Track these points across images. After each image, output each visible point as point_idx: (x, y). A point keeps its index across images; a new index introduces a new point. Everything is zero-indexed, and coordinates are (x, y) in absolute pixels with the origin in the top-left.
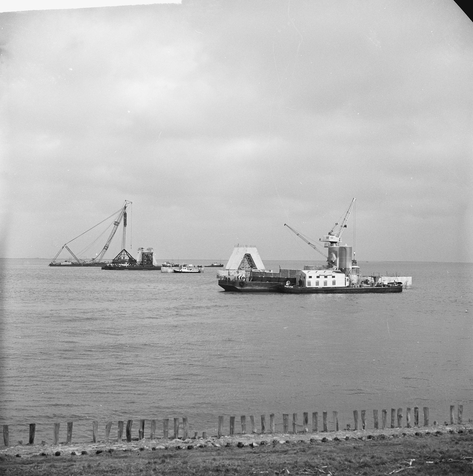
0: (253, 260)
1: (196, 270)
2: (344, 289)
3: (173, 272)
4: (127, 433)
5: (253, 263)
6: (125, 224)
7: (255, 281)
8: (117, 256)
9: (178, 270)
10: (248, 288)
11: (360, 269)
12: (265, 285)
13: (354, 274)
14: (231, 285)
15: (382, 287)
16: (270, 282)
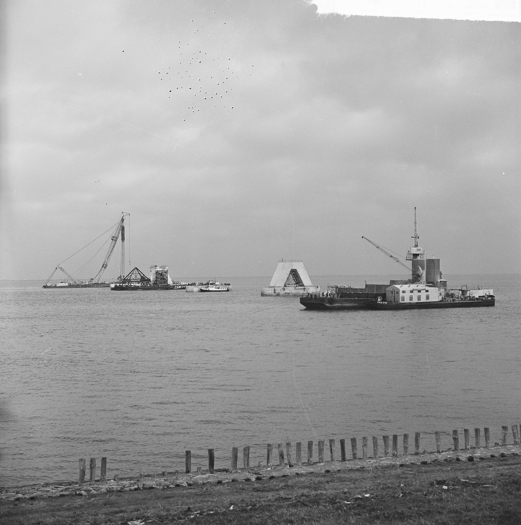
0: (299, 276)
1: (224, 288)
2: (438, 304)
3: (199, 291)
5: (299, 279)
6: (123, 239)
9: (205, 289)
12: (355, 301)
13: (442, 287)
16: (358, 298)
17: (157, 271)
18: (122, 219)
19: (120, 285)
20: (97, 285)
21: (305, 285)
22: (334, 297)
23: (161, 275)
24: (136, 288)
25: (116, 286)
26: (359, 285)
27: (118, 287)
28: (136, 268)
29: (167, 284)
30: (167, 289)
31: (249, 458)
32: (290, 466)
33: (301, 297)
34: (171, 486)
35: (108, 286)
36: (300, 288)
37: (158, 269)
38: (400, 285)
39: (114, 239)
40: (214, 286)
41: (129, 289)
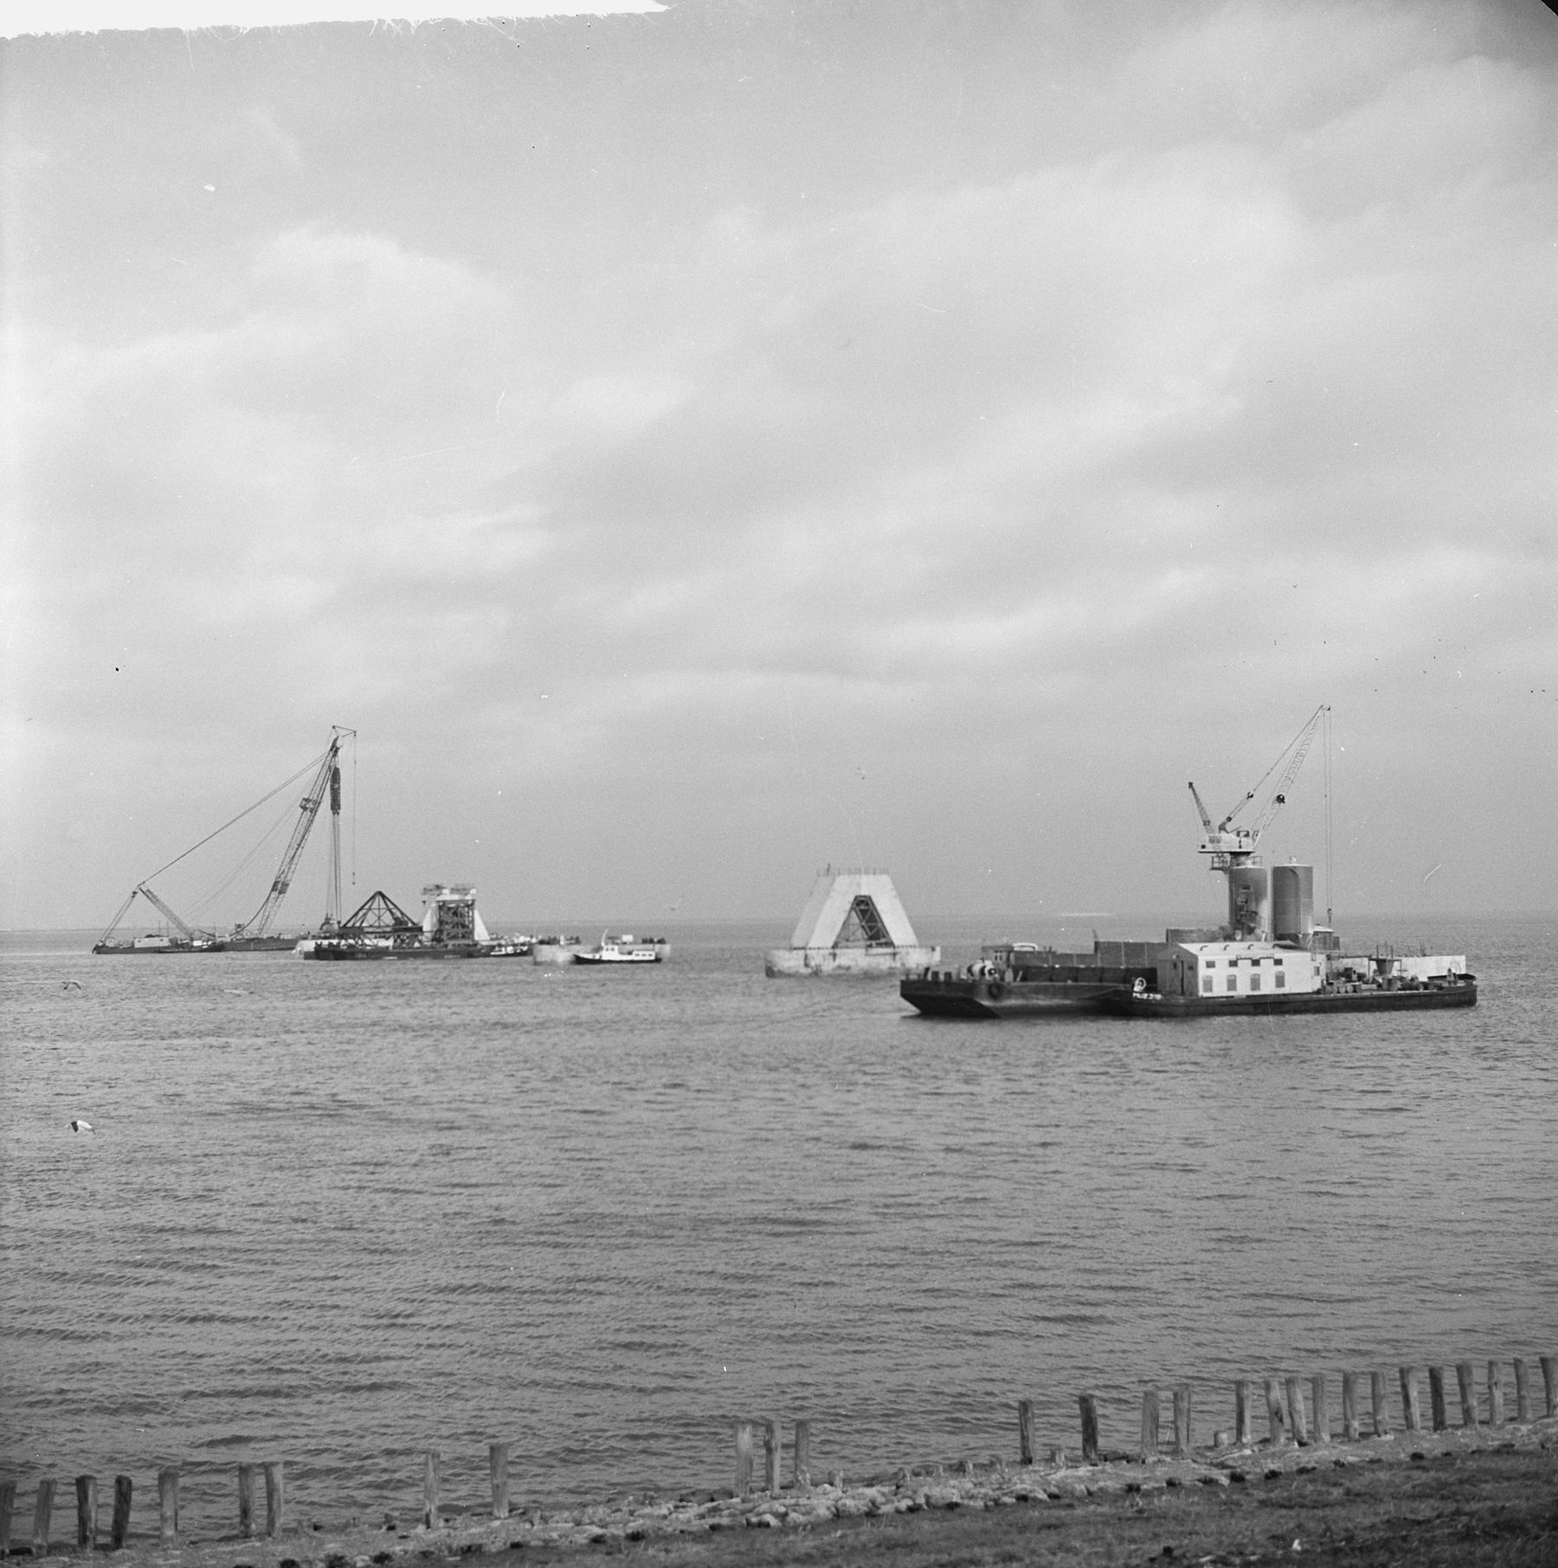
4: (1442, 1388)
5: (880, 925)
6: (335, 806)
7: (1033, 980)
8: (357, 914)
9: (589, 956)
12: (1065, 992)
14: (961, 994)
15: (1421, 991)
17: (444, 902)
19: (330, 944)
20: (255, 944)
21: (896, 943)
22: (1002, 979)
24: (377, 954)
25: (318, 947)
26: (1074, 943)
27: (325, 950)
28: (380, 893)
30: (470, 955)
31: (1157, 1427)
35: (289, 945)
37: (447, 896)
38: (1200, 945)
39: (310, 805)
40: (616, 947)
41: (360, 956)
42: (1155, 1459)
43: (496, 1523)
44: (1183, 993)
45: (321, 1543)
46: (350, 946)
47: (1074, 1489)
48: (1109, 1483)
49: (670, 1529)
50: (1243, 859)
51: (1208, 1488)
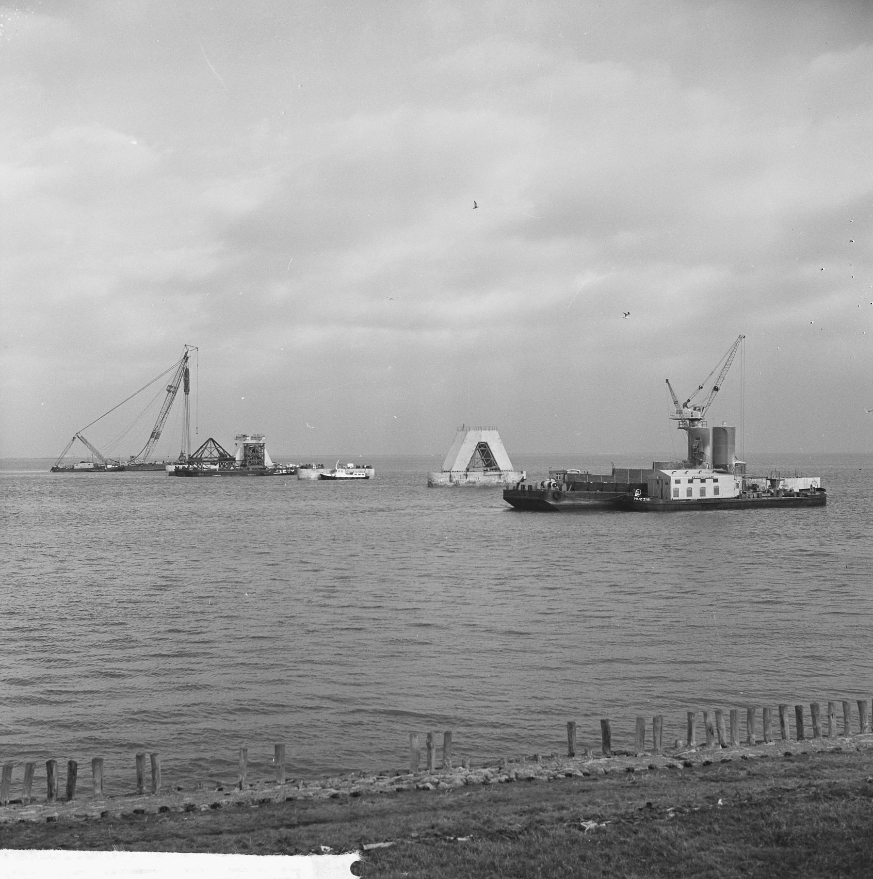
5: (492, 459)
6: (187, 390)
8: (198, 451)
9: (329, 475)
10: (566, 502)
11: (747, 466)
12: (596, 497)
18: (185, 357)
22: (561, 489)
23: (254, 451)
24: (211, 473)
25: (177, 469)
27: (180, 471)
28: (211, 439)
29: (264, 466)
30: (262, 474)
32: (723, 747)
33: (505, 489)
34: (560, 776)
35: (161, 468)
36: (492, 473)
37: (249, 441)
39: (172, 389)
42: (642, 754)
43: (279, 787)
44: (662, 498)
45: (182, 797)
46: (195, 469)
47: (597, 770)
48: (617, 767)
49: (374, 791)
50: (696, 422)
51: (672, 771)
